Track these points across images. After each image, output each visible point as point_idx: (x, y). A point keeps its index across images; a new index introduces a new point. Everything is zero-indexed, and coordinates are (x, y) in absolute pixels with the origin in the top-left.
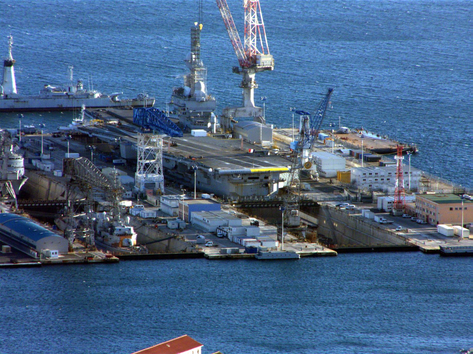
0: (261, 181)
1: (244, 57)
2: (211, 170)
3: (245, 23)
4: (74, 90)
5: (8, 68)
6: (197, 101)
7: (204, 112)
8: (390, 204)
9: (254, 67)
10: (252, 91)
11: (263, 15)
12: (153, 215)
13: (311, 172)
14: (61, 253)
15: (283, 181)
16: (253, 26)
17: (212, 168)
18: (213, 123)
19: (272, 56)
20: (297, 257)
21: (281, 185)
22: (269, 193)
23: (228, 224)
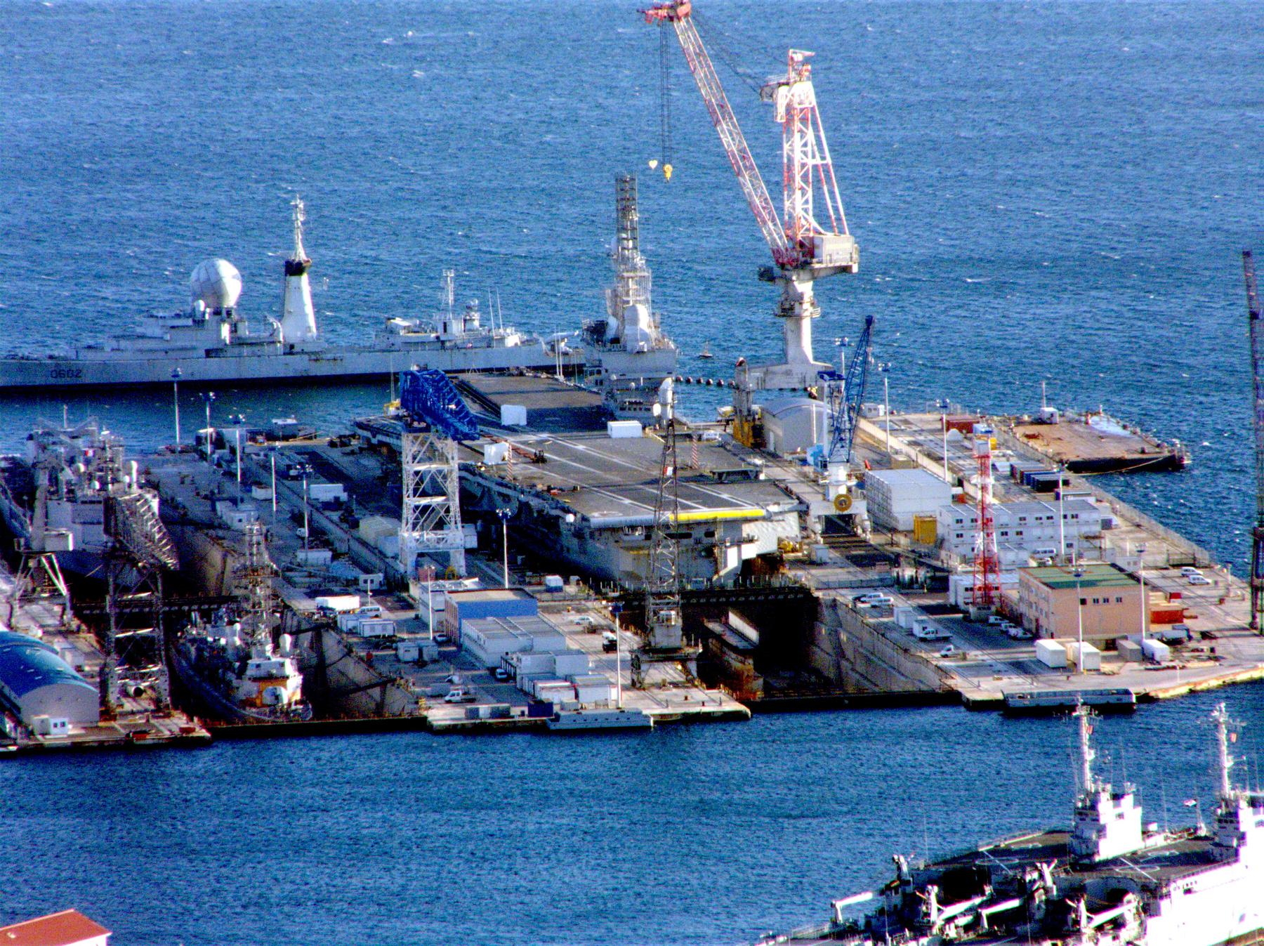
0: (698, 542)
1: (782, 243)
2: (570, 518)
3: (785, 160)
4: (457, 328)
5: (293, 279)
6: (631, 353)
8: (970, 593)
9: (808, 267)
10: (806, 326)
11: (827, 138)
12: (384, 629)
14: (76, 723)
15: (751, 541)
16: (803, 165)
17: (575, 514)
19: (852, 239)
20: (646, 724)
21: (750, 552)
22: (717, 572)
23: (532, 647)
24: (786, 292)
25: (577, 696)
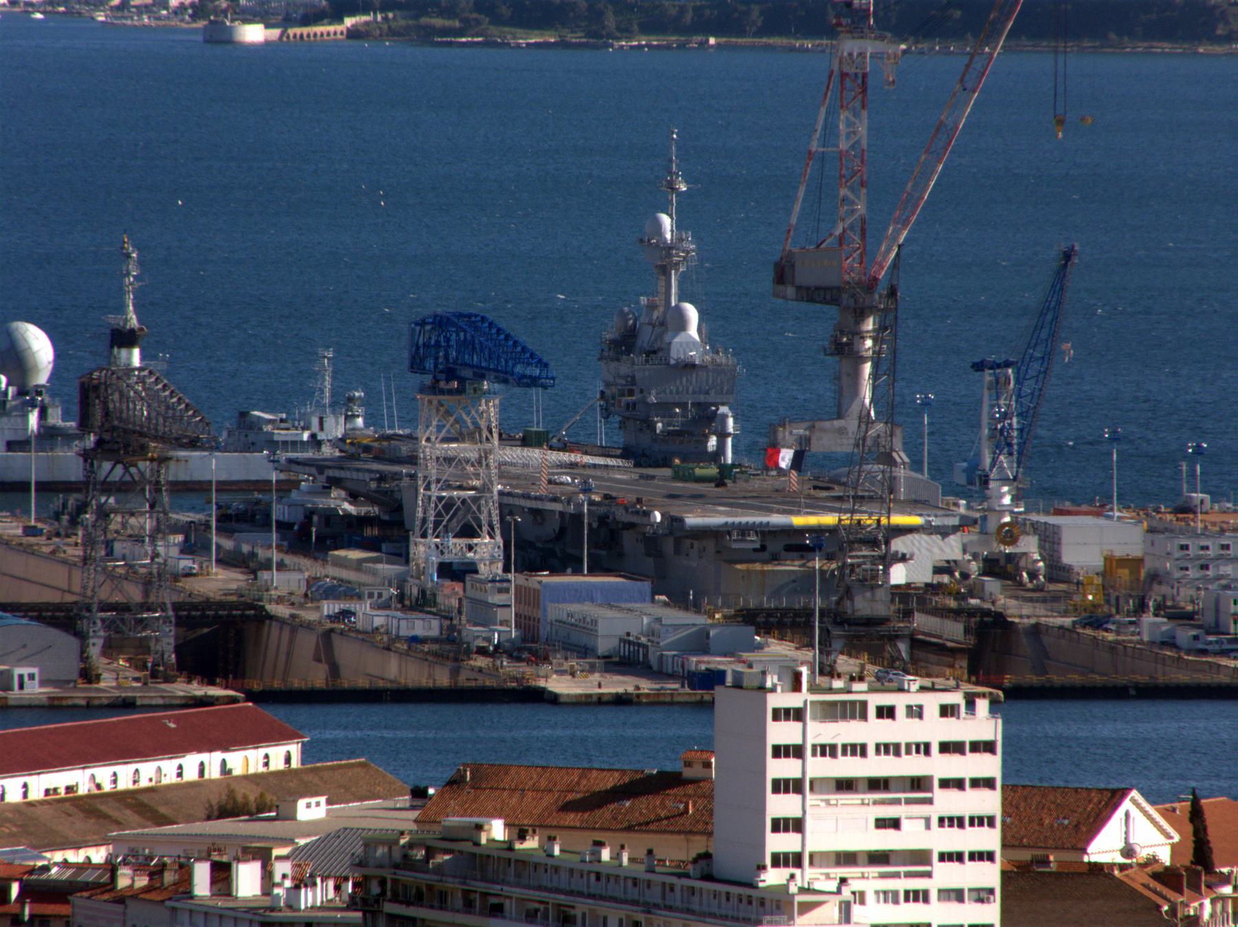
7: (1059, 863)
13: (1023, 563)
18: (722, 436)
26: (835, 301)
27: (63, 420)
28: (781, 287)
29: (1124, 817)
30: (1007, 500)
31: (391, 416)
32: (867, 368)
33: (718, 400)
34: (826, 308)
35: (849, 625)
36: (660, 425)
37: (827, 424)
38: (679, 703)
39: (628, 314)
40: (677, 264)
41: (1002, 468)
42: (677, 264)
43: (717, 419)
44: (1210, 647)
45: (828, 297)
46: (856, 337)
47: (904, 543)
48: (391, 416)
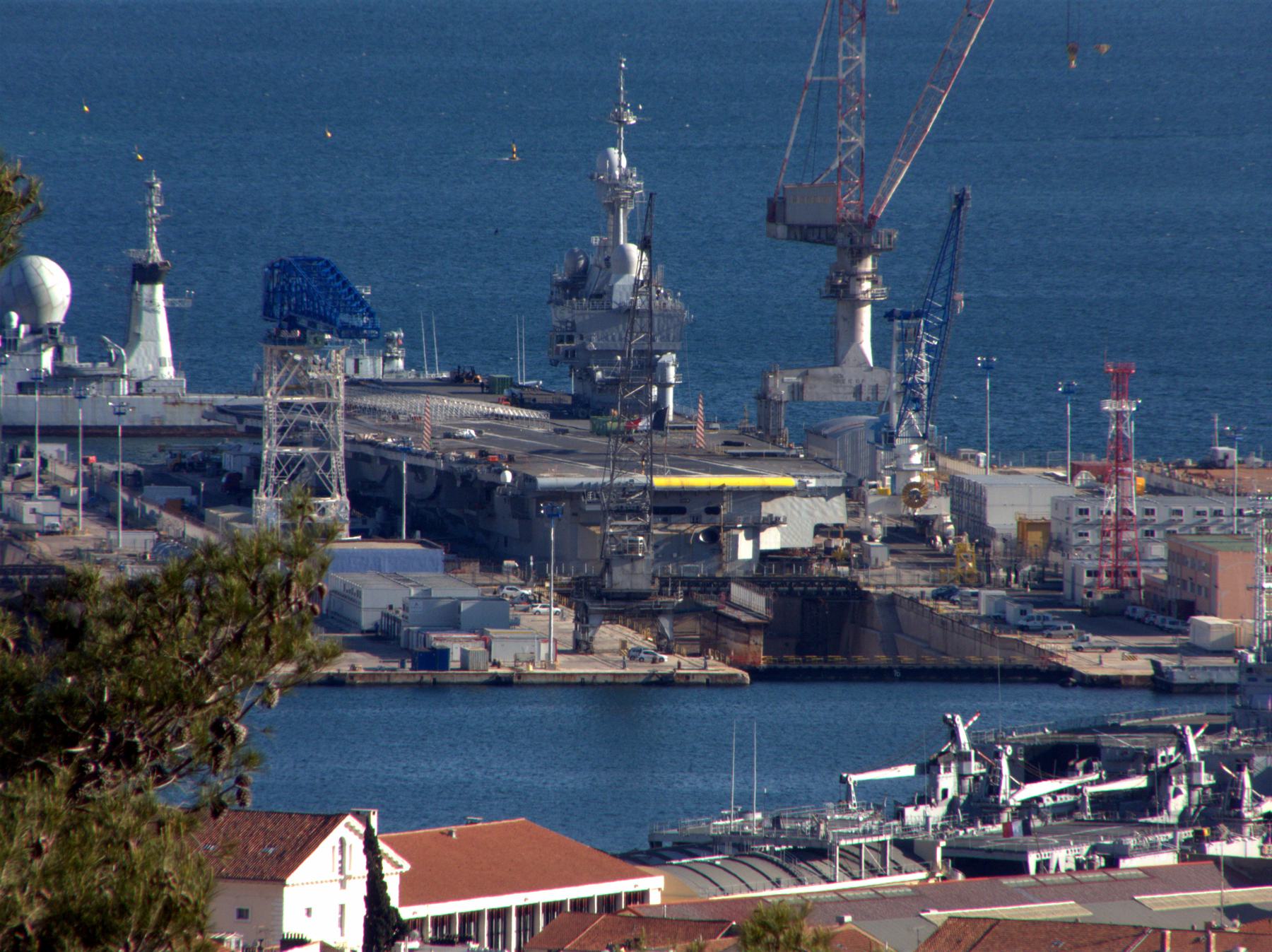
18: (663, 386)
24: (903, 825)
25: (488, 647)
26: (831, 241)
27: (80, 360)
28: (772, 226)
29: (338, 845)
30: (916, 459)
31: (431, 355)
32: (866, 313)
33: (663, 348)
34: (819, 248)
35: (608, 599)
36: (599, 374)
37: (821, 371)
38: (396, 684)
39: (578, 254)
40: (625, 202)
41: (910, 425)
42: (625, 202)
43: (658, 369)
44: (1031, 624)
45: (823, 236)
46: (853, 279)
47: (783, 506)
48: (431, 355)
